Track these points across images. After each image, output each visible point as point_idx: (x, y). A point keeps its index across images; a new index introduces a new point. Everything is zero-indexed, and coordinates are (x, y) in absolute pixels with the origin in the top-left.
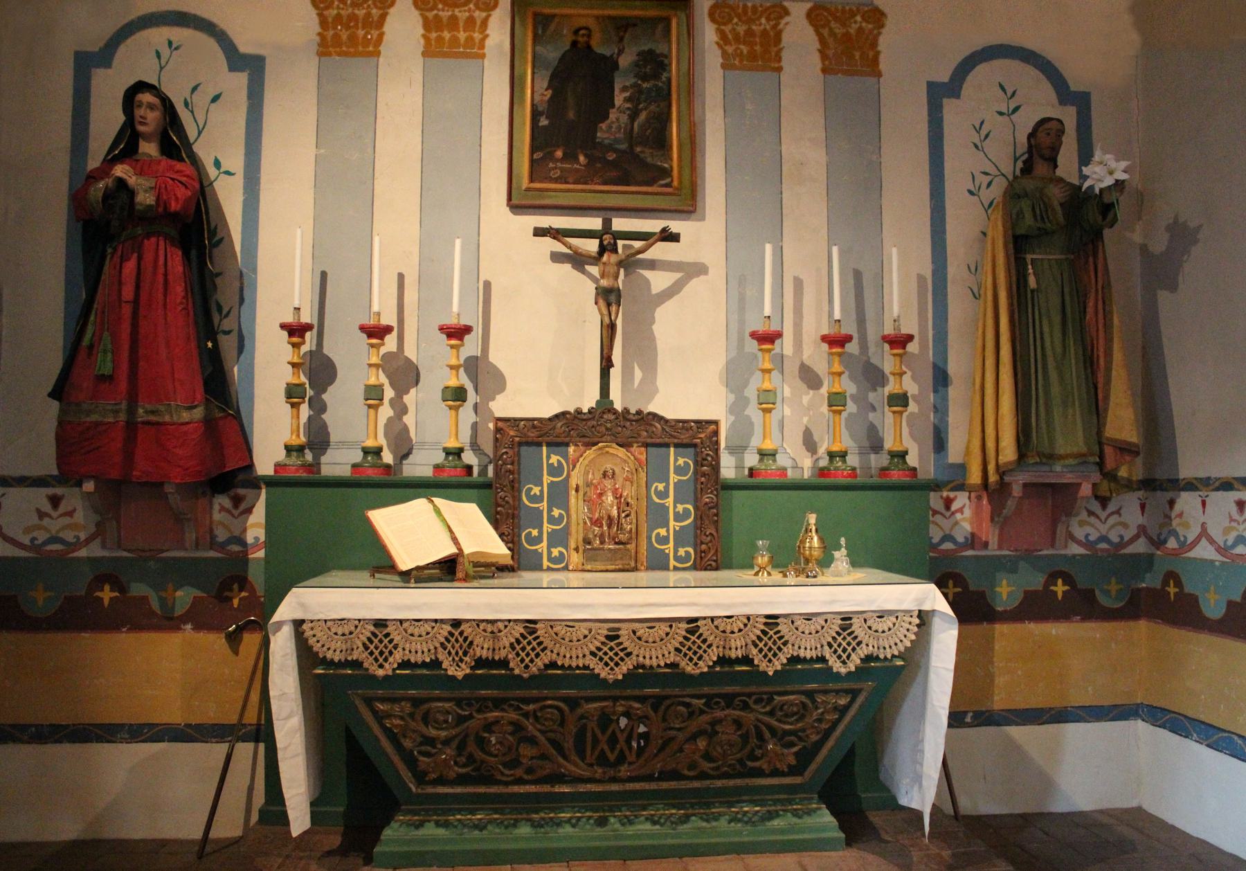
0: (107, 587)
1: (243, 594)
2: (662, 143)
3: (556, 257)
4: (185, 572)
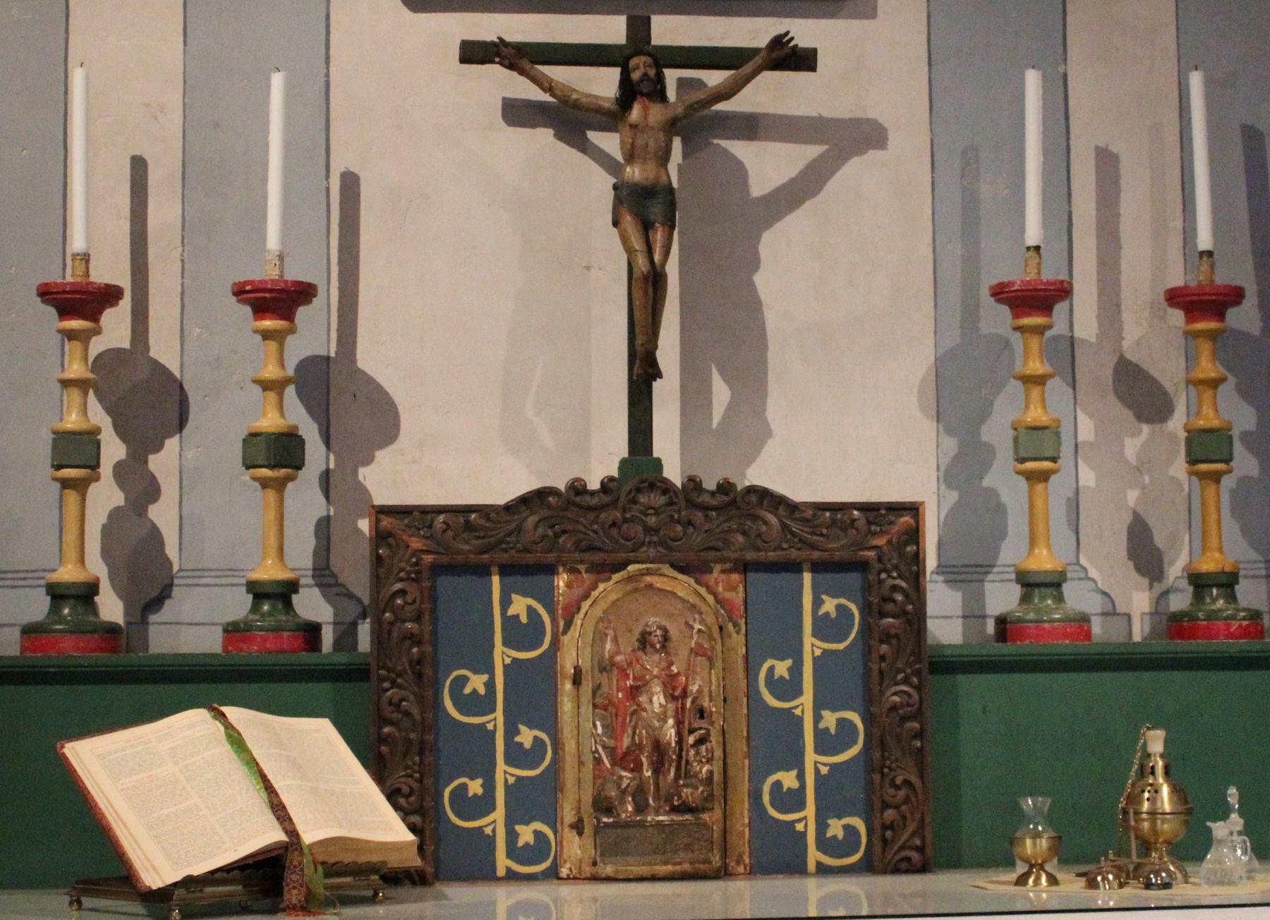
3: (516, 113)
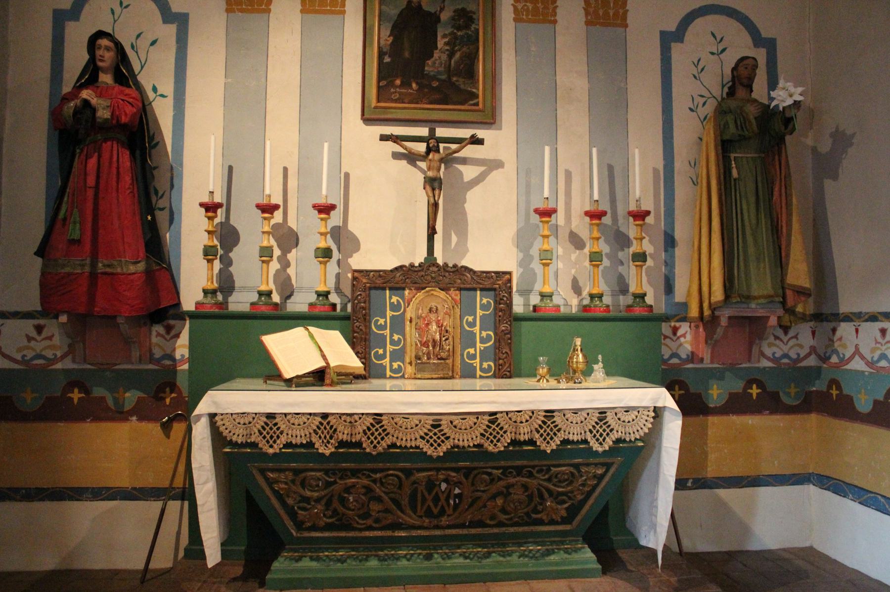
0: (76, 390)
1: (173, 395)
2: (471, 74)
3: (396, 156)
4: (133, 380)
